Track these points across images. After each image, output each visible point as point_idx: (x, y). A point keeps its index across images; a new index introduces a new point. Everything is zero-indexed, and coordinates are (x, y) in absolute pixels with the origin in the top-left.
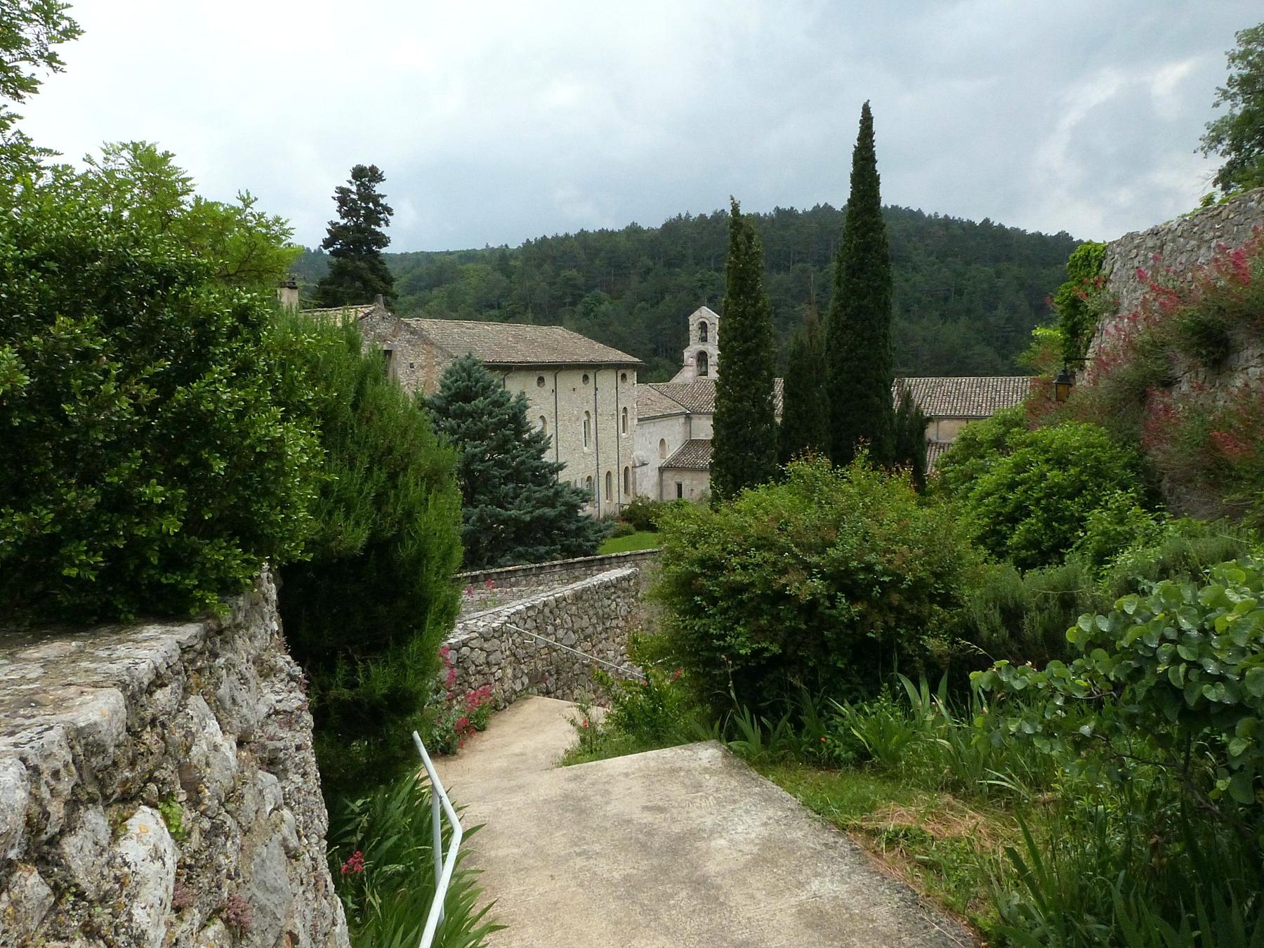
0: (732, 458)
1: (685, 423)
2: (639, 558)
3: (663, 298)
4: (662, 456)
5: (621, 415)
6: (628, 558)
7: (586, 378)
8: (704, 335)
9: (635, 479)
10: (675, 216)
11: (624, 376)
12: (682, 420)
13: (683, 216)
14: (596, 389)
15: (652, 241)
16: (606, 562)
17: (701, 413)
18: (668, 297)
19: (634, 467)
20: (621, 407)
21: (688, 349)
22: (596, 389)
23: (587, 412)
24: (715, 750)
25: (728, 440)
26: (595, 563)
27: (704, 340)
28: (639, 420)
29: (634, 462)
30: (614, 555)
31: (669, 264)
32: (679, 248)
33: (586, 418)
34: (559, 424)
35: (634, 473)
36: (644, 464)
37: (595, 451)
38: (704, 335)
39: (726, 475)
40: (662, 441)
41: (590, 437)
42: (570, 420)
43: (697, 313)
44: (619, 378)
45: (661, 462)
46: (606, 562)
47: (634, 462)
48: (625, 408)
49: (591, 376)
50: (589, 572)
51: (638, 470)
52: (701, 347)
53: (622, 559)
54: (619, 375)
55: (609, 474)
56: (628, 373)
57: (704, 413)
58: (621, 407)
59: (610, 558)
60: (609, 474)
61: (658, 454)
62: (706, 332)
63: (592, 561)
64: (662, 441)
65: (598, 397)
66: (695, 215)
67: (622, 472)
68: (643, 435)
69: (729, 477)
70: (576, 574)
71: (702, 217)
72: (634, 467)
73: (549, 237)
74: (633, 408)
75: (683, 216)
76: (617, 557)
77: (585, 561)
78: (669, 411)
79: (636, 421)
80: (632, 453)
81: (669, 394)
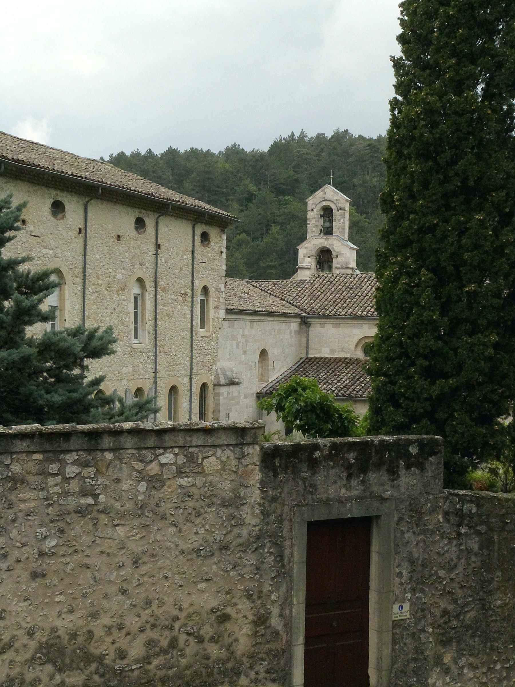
0: (432, 229)
1: (299, 332)
2: (197, 440)
3: (268, 230)
4: (262, 378)
5: (199, 298)
6: (168, 439)
7: (140, 224)
8: (327, 224)
9: (217, 405)
10: (286, 135)
11: (205, 237)
12: (294, 326)
13: (297, 135)
14: (158, 247)
15: (257, 161)
16: (107, 442)
17: (324, 317)
18: (275, 229)
19: (217, 385)
20: (199, 285)
21: (305, 244)
22: (158, 247)
23: (140, 281)
24: (135, 439)
25: (425, 185)
26: (74, 443)
27: (328, 232)
28: (229, 312)
29: (217, 377)
30: (128, 425)
31: (279, 191)
32: (291, 172)
33: (137, 290)
34: (90, 289)
35: (217, 395)
36: (232, 383)
37: (151, 346)
38: (327, 224)
39: (417, 272)
40: (263, 353)
41: (144, 323)
42: (109, 287)
43: (319, 194)
44: (198, 238)
45: (257, 387)
46: (107, 442)
47: (217, 377)
48: (205, 289)
49: (150, 222)
50: (54, 467)
51: (223, 390)
52: (322, 242)
53: (151, 441)
54: (198, 232)
55: (173, 390)
56: (213, 232)
57: (329, 317)
58: (199, 285)
59: (118, 433)
60: (173, 390)
61: (256, 372)
62: (331, 221)
63: (67, 435)
64: (263, 353)
65: (162, 260)
66: (311, 134)
67: (196, 389)
68: (234, 337)
69: (425, 275)
70: (16, 468)
71: (320, 137)
72: (217, 385)
73: (128, 153)
74: (218, 290)
75: (297, 135)
76: (135, 432)
77: (41, 434)
78: (274, 309)
79: (222, 313)
80: (214, 363)
81: (276, 292)
